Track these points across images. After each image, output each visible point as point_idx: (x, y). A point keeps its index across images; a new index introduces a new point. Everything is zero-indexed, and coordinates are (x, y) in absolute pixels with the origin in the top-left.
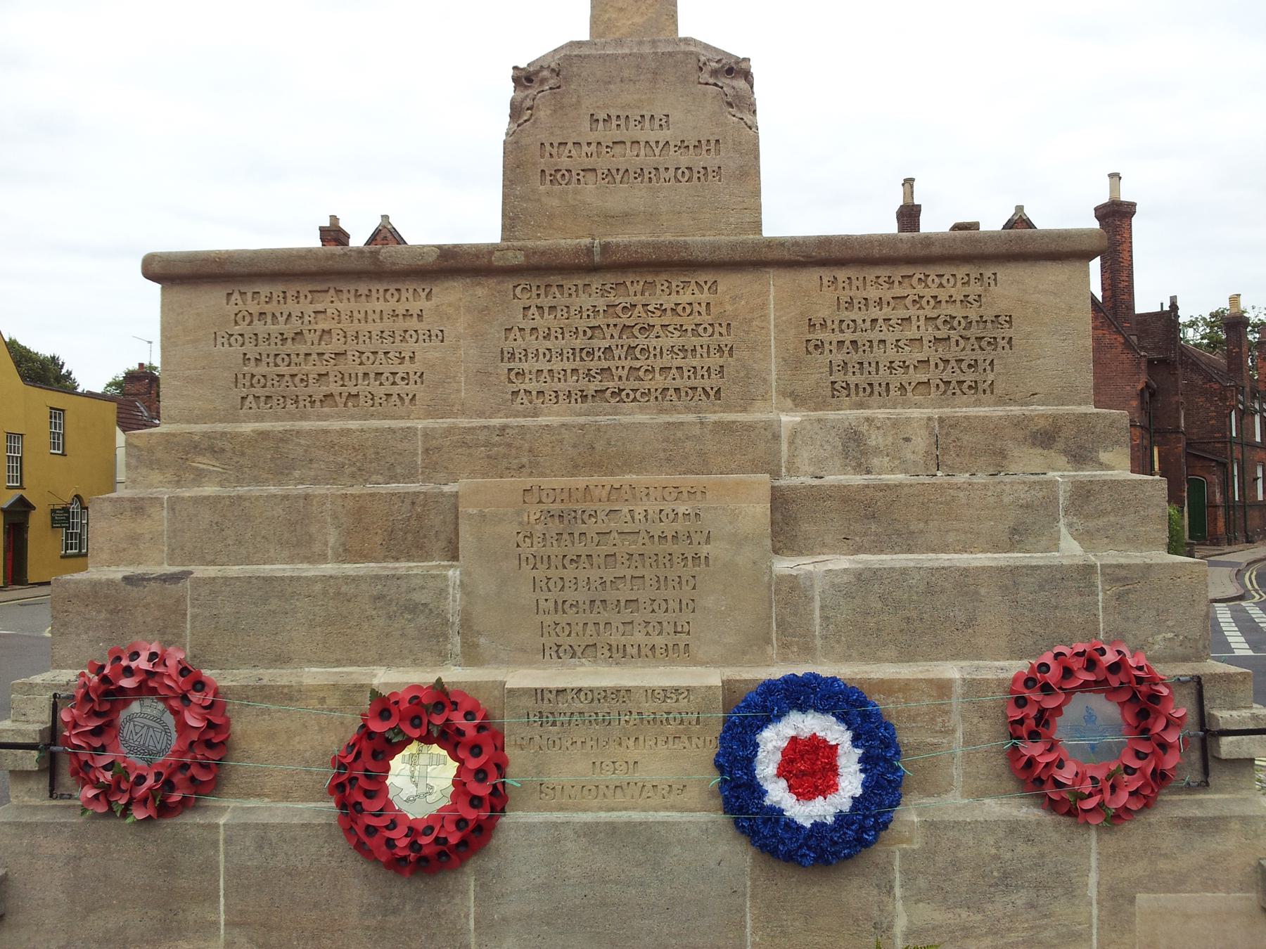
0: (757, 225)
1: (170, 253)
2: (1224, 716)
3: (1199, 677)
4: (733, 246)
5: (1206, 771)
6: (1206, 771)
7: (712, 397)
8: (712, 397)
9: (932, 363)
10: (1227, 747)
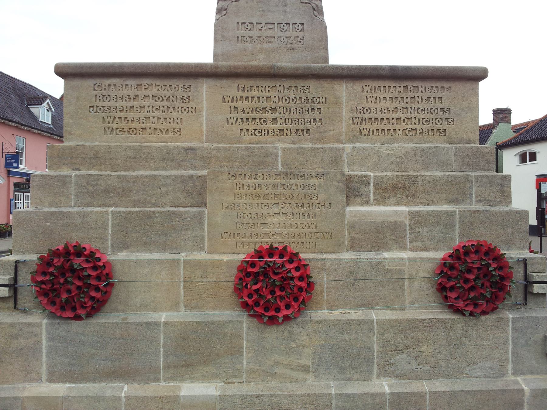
0: (326, 59)
1: (448, 67)
2: (535, 276)
3: (526, 260)
4: (305, 68)
5: (526, 299)
6: (526, 299)
7: (164, 133)
8: (164, 133)
9: (402, 120)
10: (537, 289)
